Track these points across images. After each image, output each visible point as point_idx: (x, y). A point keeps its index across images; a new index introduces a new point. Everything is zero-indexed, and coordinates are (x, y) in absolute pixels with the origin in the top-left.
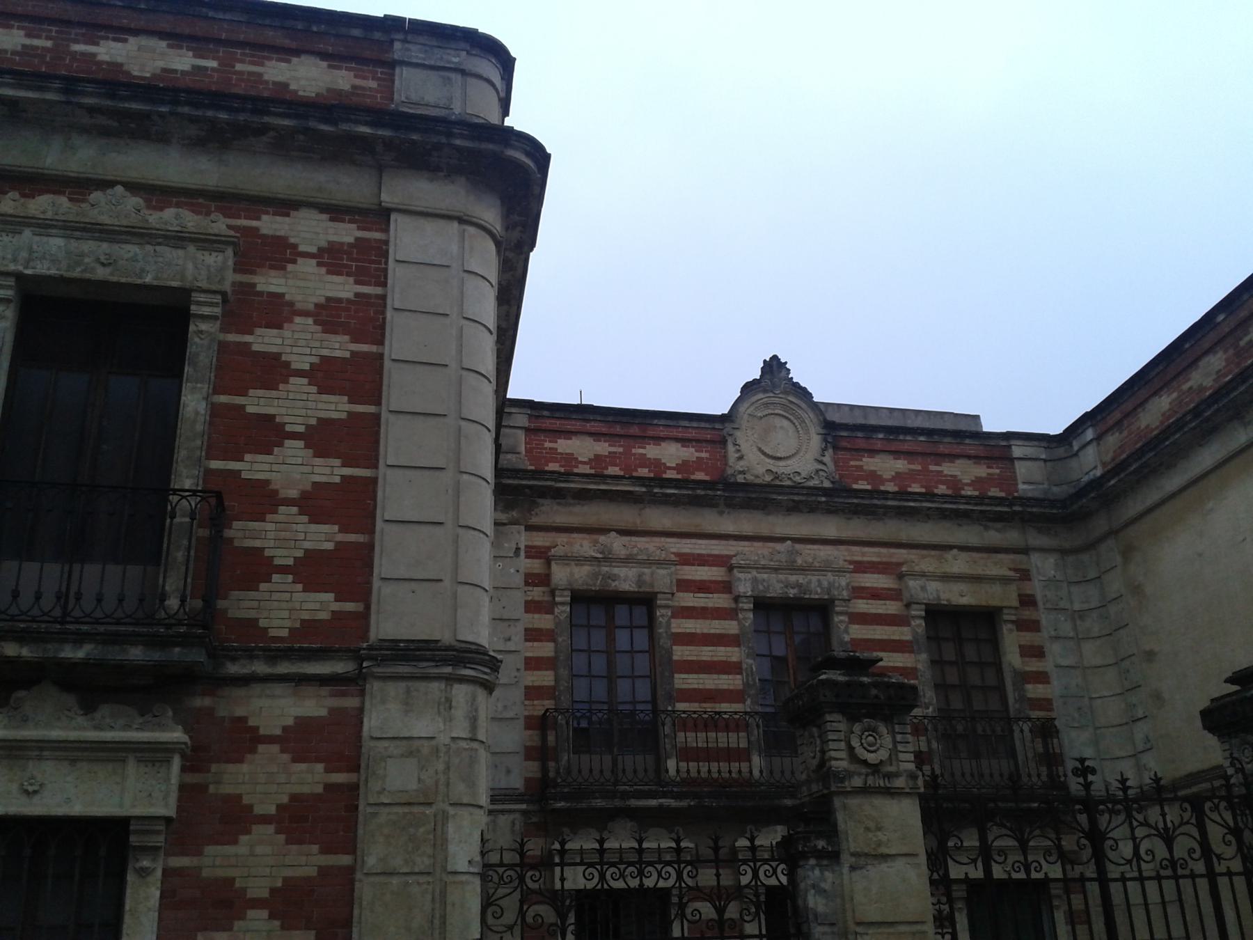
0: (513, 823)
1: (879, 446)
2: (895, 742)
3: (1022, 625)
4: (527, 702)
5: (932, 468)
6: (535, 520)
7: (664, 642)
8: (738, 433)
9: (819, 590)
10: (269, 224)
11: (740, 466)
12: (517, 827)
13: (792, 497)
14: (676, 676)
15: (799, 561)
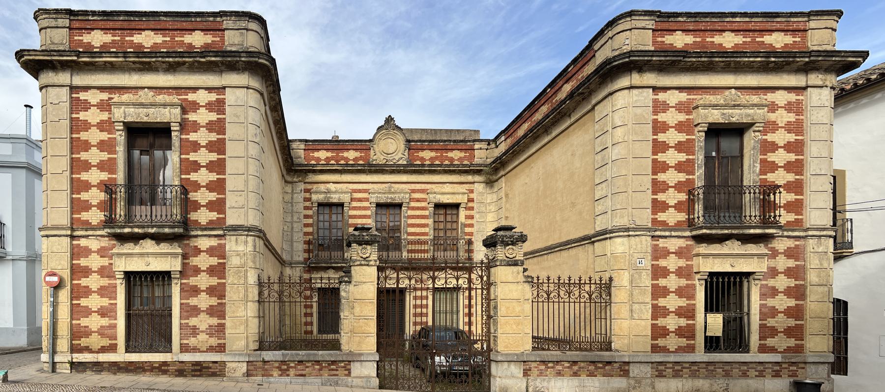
7: (346, 218)
10: (191, 97)
11: (375, 158)
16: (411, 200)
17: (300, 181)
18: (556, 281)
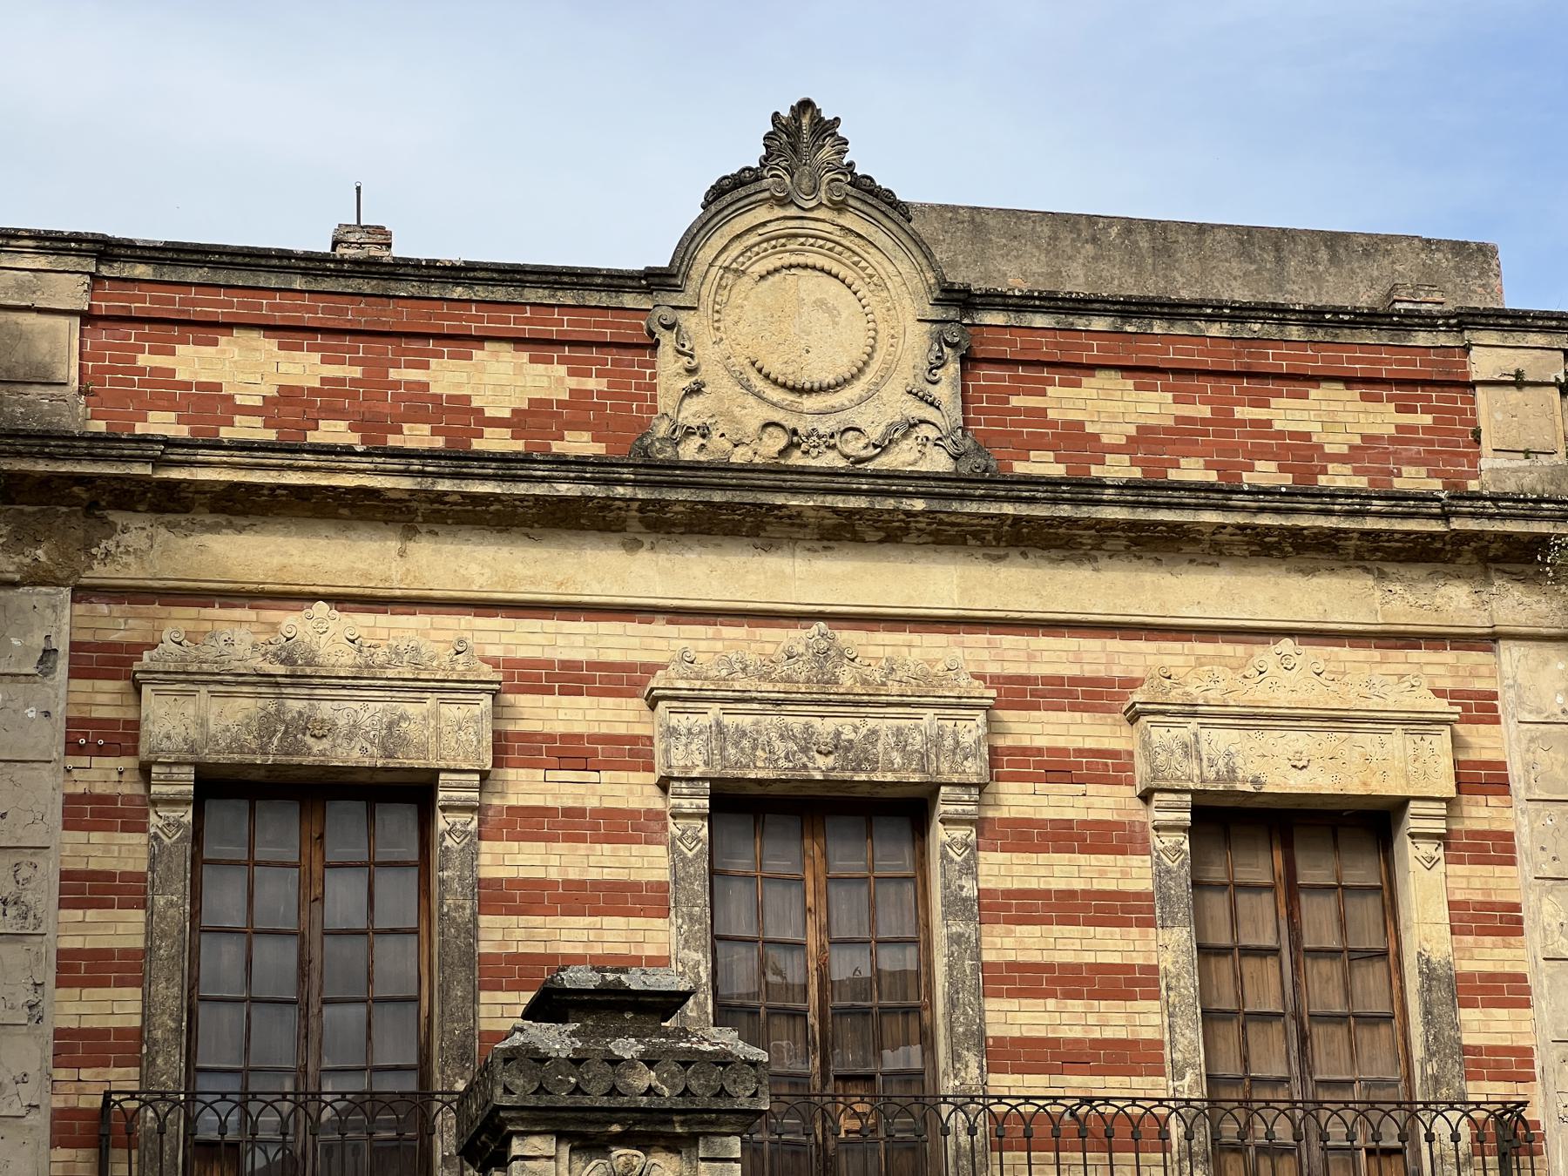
1: (1094, 353)
4: (61, 1074)
5: (1243, 413)
6: (101, 573)
7: (454, 902)
8: (688, 321)
9: (898, 760)
11: (692, 413)
13: (830, 500)
14: (485, 996)
15: (847, 679)
16: (1005, 763)
17: (37, 578)
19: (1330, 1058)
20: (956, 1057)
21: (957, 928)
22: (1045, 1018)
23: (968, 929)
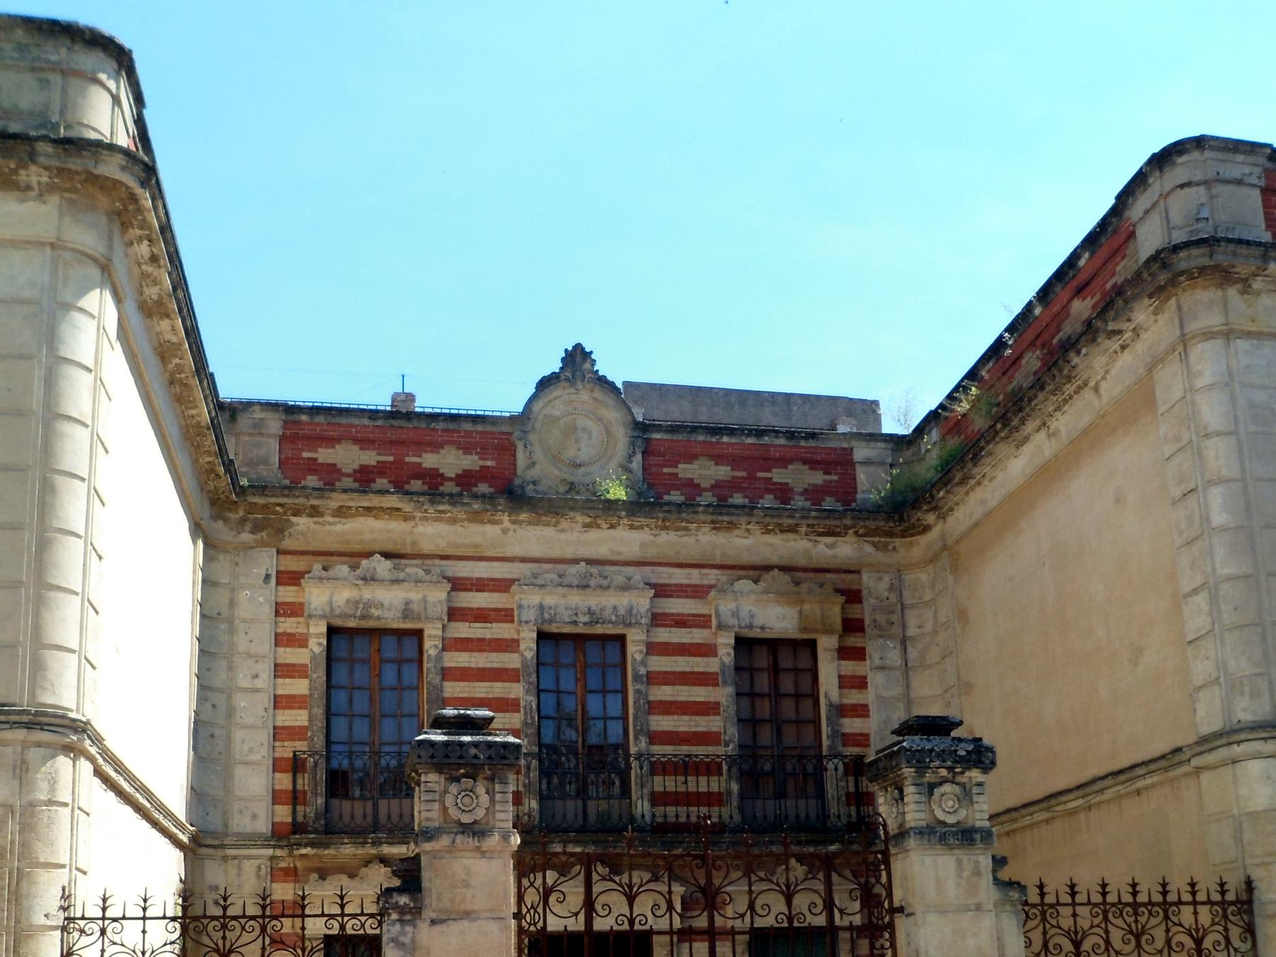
0: (259, 868)
2: (492, 801)
3: (846, 653)
11: (535, 473)
12: (263, 872)
16: (658, 619)
17: (263, 544)
18: (1097, 898)
19: (789, 738)
20: (636, 738)
21: (638, 687)
22: (672, 723)
23: (643, 688)
